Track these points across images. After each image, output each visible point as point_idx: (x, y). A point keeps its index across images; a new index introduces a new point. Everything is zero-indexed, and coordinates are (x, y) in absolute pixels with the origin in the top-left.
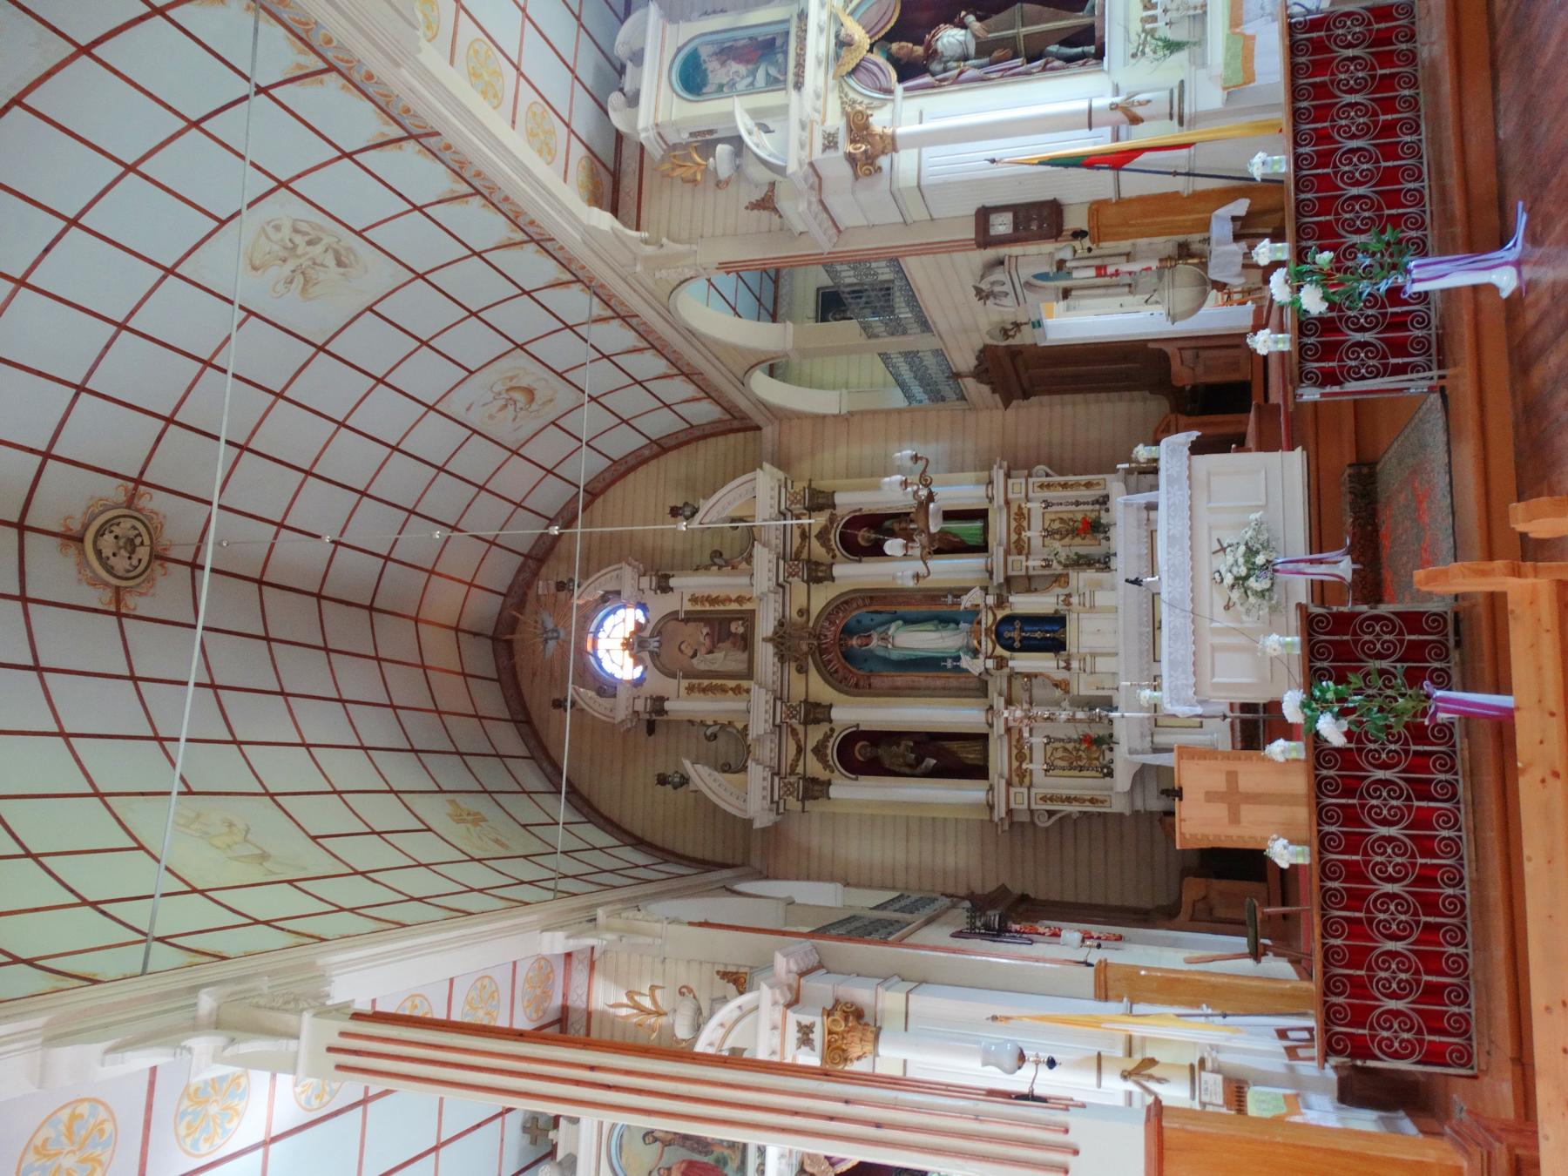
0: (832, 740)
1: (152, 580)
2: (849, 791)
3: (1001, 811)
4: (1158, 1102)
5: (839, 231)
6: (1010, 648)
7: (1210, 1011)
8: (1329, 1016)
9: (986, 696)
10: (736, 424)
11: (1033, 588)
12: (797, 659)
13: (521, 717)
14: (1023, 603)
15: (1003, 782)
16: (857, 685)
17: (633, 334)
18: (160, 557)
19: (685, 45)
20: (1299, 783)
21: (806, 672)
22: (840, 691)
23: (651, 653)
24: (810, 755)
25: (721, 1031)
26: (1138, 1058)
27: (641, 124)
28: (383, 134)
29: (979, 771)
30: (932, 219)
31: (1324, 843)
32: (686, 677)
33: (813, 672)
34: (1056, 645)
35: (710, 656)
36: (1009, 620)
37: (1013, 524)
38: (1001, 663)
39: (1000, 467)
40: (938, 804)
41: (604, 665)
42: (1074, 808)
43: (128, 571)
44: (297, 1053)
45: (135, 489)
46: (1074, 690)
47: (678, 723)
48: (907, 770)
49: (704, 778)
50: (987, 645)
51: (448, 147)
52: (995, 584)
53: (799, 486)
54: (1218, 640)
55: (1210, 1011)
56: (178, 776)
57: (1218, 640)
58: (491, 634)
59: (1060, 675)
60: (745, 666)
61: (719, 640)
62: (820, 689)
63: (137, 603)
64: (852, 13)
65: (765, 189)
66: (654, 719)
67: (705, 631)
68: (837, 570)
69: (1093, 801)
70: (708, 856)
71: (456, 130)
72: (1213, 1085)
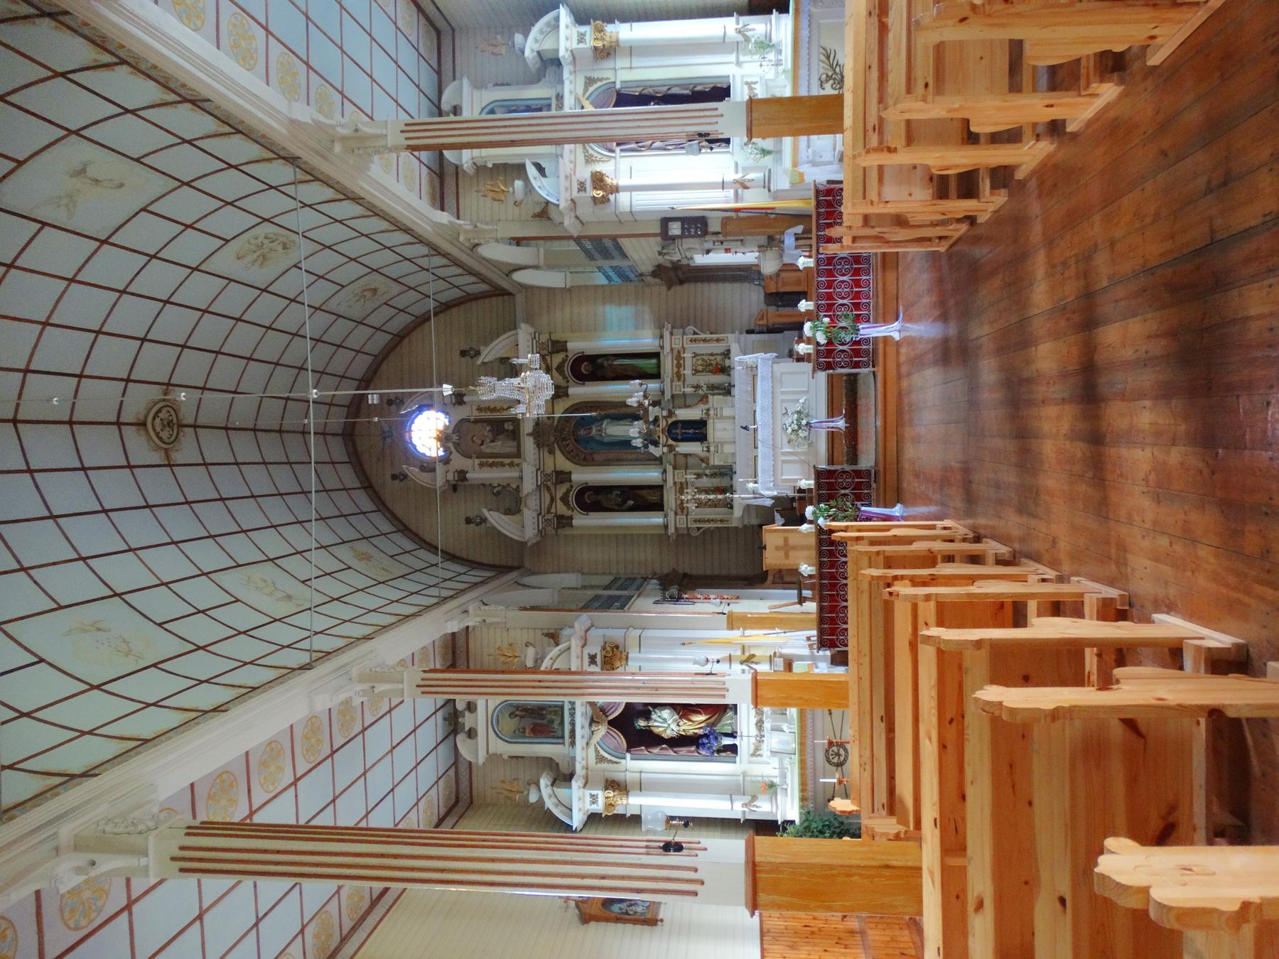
0: (572, 492)
2: (585, 521)
3: (671, 530)
4: (756, 670)
5: (583, 224)
6: (675, 440)
7: (779, 631)
8: (821, 632)
9: (662, 464)
10: (497, 292)
11: (688, 404)
12: (548, 446)
13: (366, 485)
14: (683, 414)
15: (673, 513)
16: (585, 459)
18: (182, 426)
19: (486, 107)
20: (812, 541)
21: (554, 453)
22: (575, 463)
23: (454, 443)
24: (558, 501)
25: (551, 661)
26: (747, 654)
27: (464, 161)
29: (658, 506)
30: (636, 221)
31: (821, 565)
32: (478, 458)
33: (558, 453)
34: (702, 438)
35: (492, 444)
36: (675, 424)
37: (675, 362)
38: (671, 448)
39: (667, 329)
40: (634, 527)
41: (418, 448)
42: (712, 525)
44: (403, 689)
46: (711, 463)
47: (472, 486)
48: (616, 508)
49: (497, 520)
50: (663, 439)
52: (666, 399)
53: (544, 338)
54: (784, 458)
55: (779, 631)
57: (784, 458)
58: (340, 432)
59: (704, 455)
60: (516, 449)
61: (498, 435)
62: (563, 463)
63: (178, 457)
64: (587, 99)
65: (543, 205)
66: (459, 483)
67: (488, 428)
68: (572, 391)
69: (721, 521)
70: (503, 562)
72: (780, 663)
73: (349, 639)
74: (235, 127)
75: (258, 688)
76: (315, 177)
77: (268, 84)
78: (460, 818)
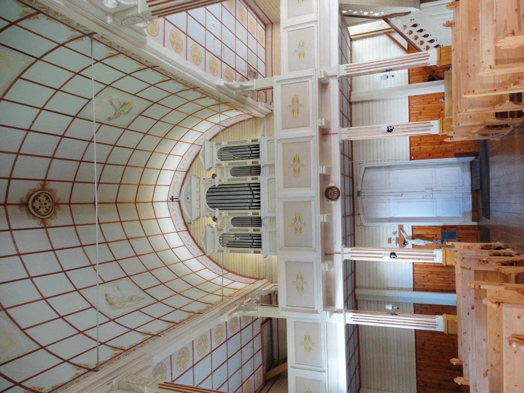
1: (55, 213)
17: (199, 93)
28: (139, 68)
43: (46, 212)
45: (44, 184)
51: (161, 69)
56: (98, 274)
71: (164, 63)
73: (246, 284)
74: (170, 78)
75: (241, 290)
76: (120, 52)
77: (164, 46)
78: (272, 386)
